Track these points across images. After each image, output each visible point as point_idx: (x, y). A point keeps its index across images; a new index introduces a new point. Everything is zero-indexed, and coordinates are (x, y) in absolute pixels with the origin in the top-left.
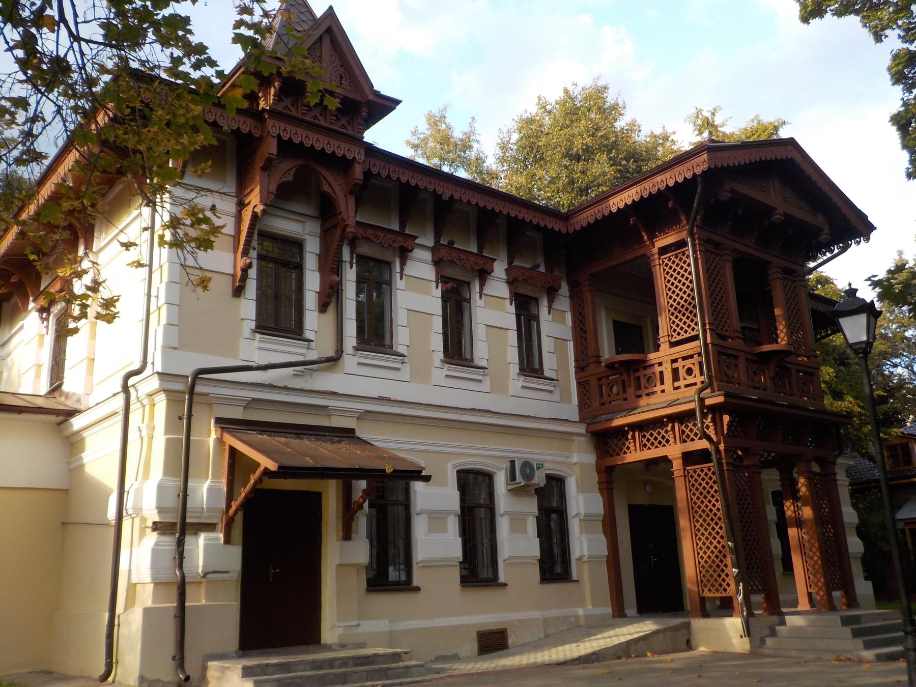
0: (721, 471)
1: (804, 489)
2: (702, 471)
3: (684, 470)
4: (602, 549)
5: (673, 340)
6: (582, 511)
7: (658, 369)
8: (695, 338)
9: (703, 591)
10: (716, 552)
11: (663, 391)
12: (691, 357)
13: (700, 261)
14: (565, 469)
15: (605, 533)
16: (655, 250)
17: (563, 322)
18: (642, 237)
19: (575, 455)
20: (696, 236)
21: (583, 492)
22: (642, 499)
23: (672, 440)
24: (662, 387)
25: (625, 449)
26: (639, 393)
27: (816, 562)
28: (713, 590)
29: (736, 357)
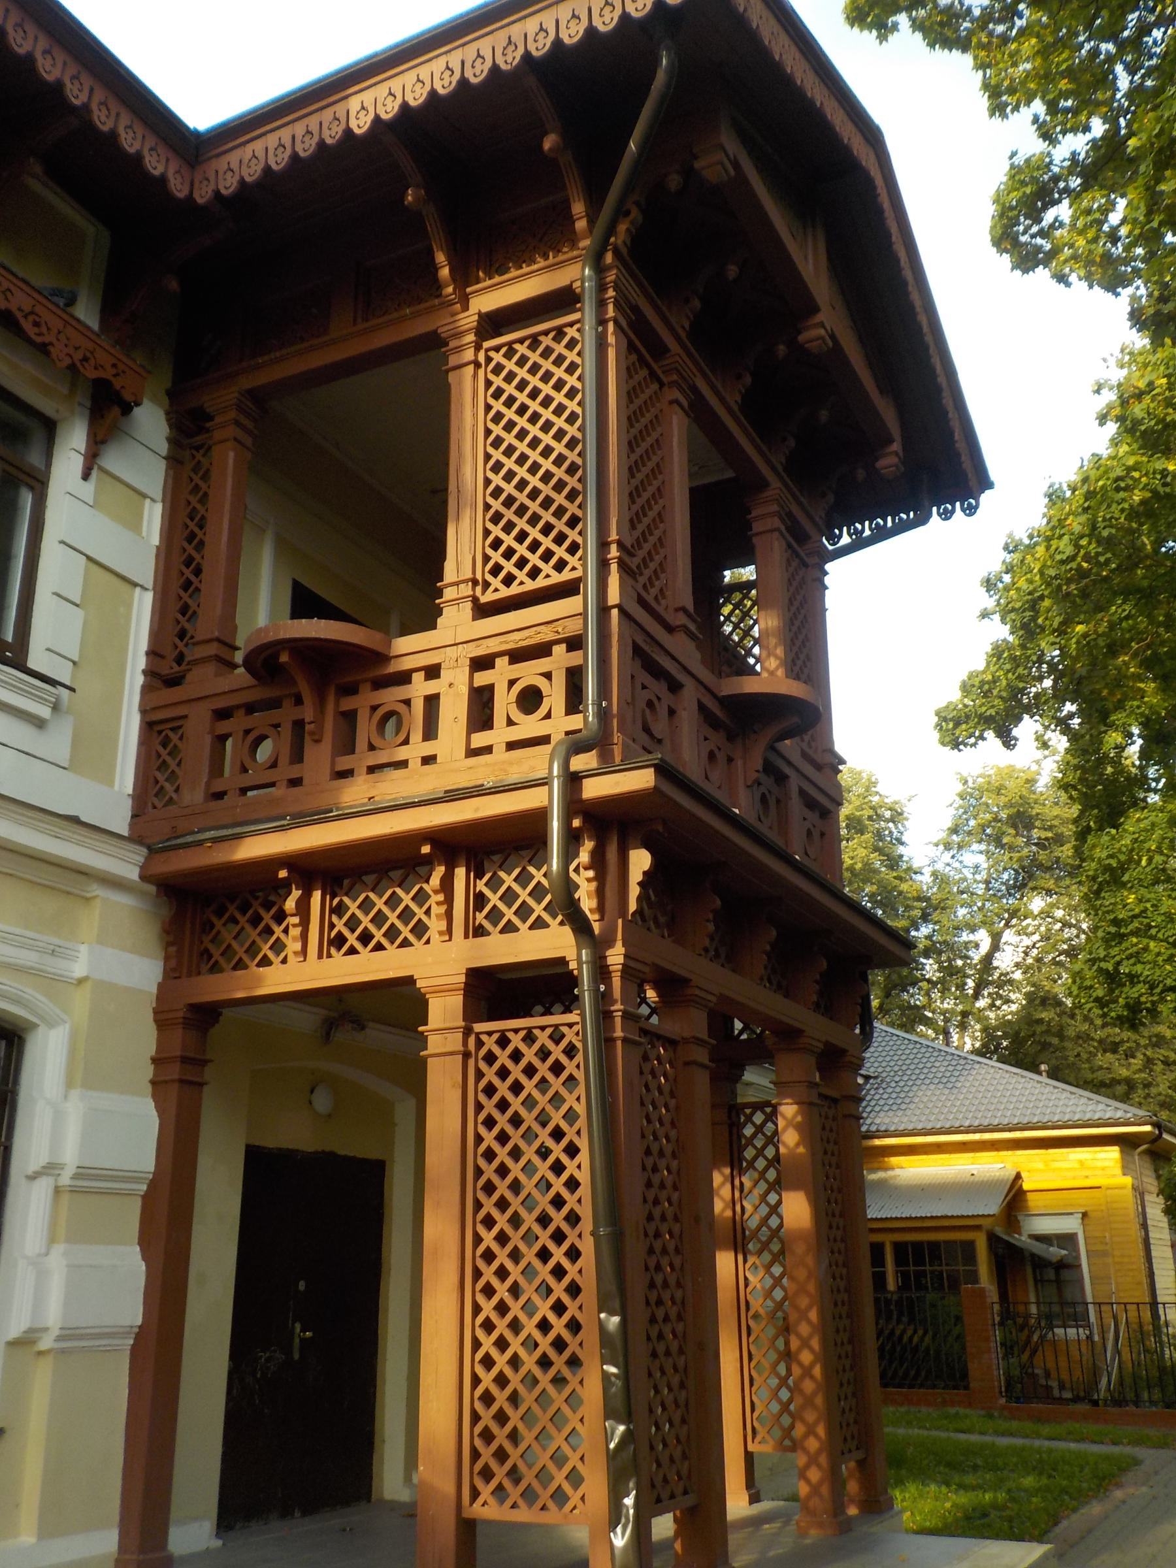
0: (605, 1042)
1: (790, 1138)
2: (529, 1038)
3: (467, 1032)
4: (124, 1300)
5: (487, 597)
6: (70, 1157)
7: (420, 688)
8: (569, 589)
9: (475, 1494)
10: (545, 1343)
11: (428, 760)
12: (542, 650)
13: (611, 353)
14: (31, 993)
15: (145, 1242)
16: (468, 319)
17: (134, 524)
18: (435, 269)
19: (84, 949)
20: (611, 277)
21: (87, 1085)
22: (295, 1133)
23: (435, 925)
24: (428, 748)
25: (266, 949)
26: (344, 763)
27: (807, 1372)
28: (514, 1493)
29: (675, 687)
